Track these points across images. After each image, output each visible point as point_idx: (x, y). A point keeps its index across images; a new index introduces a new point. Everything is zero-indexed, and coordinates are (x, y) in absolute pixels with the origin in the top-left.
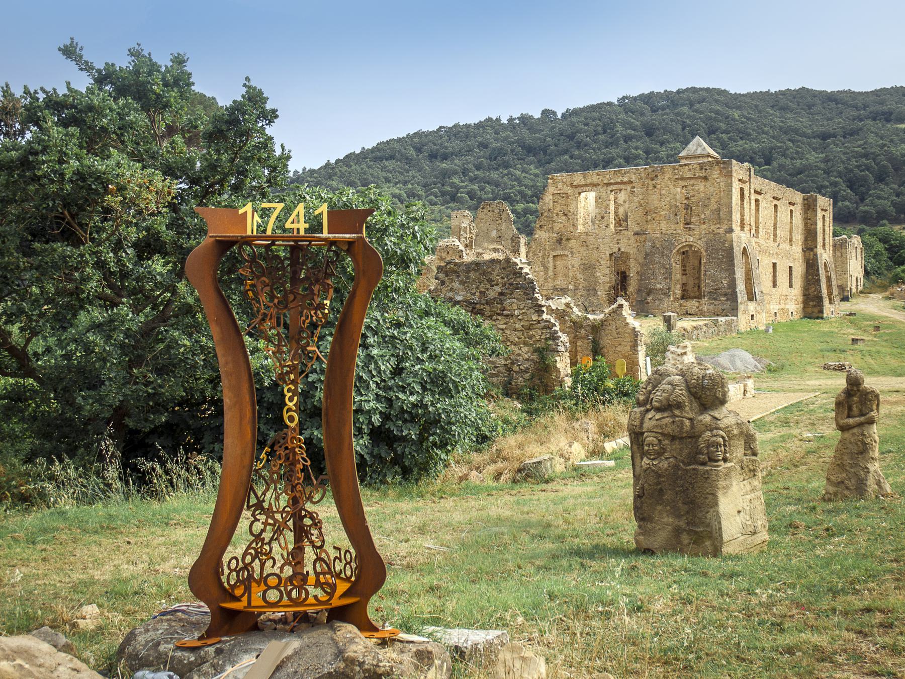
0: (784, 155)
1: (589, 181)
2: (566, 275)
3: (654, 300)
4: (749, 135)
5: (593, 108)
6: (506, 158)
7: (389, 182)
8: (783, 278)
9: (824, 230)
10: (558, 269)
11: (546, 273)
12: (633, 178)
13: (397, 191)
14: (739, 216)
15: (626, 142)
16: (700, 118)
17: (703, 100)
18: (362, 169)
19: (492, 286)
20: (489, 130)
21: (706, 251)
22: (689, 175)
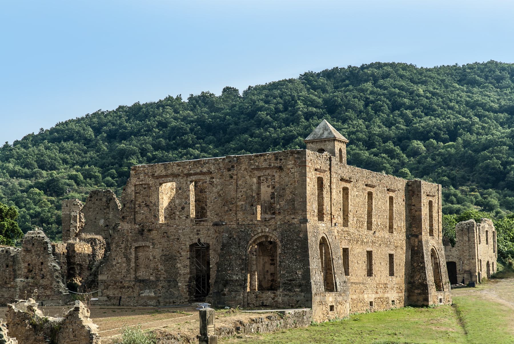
0: (470, 130)
1: (169, 172)
2: (147, 267)
3: (230, 291)
4: (435, 110)
5: (274, 86)
6: (185, 137)
7: (67, 163)
8: (381, 267)
9: (431, 217)
10: (140, 261)
11: (129, 265)
12: (213, 168)
13: (74, 173)
14: (315, 206)
15: (307, 119)
16: (384, 95)
18: (39, 150)
20: (169, 109)
21: (281, 241)
22: (264, 165)
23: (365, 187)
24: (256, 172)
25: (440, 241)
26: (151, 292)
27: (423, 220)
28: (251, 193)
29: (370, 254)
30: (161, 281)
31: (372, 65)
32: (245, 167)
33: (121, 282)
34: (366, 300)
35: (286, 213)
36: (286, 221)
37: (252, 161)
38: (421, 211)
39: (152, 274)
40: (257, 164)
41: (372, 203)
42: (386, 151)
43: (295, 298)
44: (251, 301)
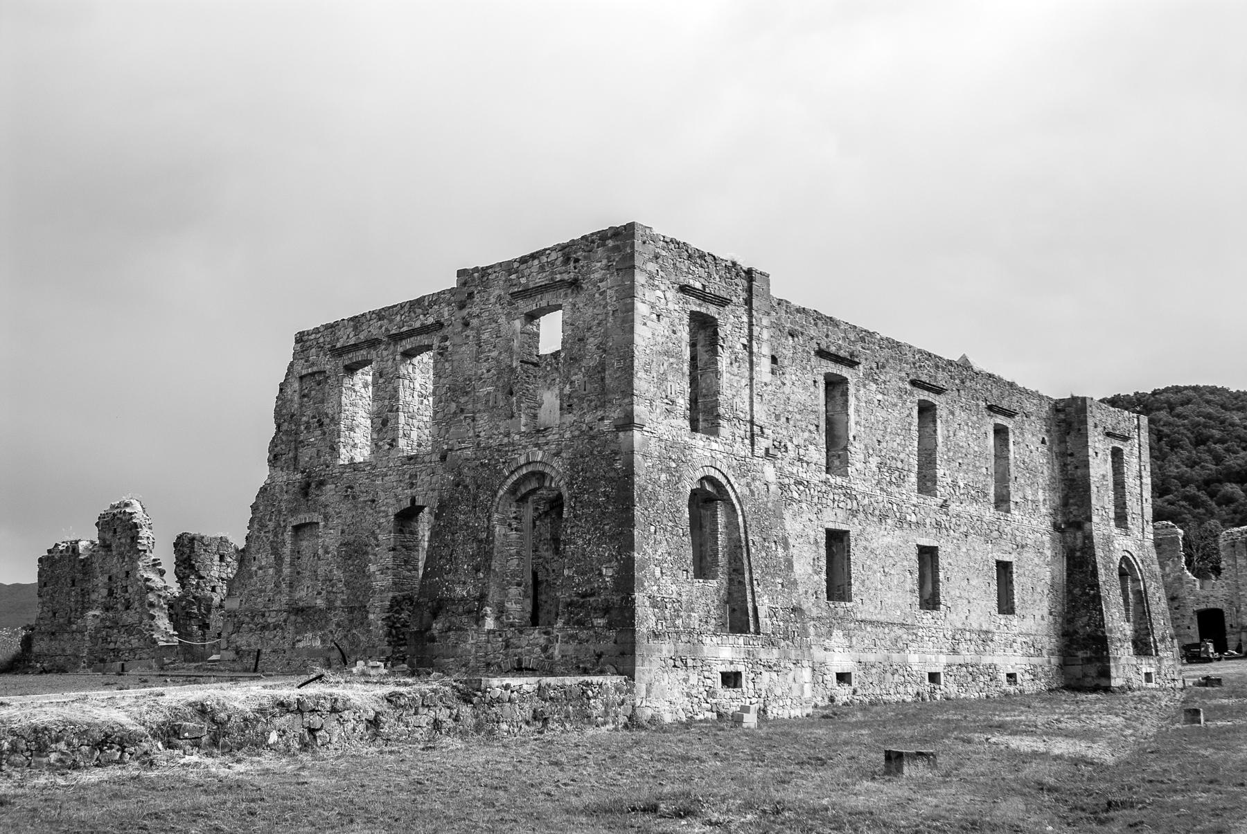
9: (1119, 485)
11: (279, 571)
16: (1183, 425)
17: (1189, 401)
22: (540, 279)
23: (908, 387)
24: (521, 303)
25: (1149, 543)
26: (314, 638)
27: (1093, 488)
28: (508, 361)
29: (928, 555)
30: (336, 608)
31: (1167, 390)
32: (497, 292)
33: (263, 615)
34: (915, 668)
35: (585, 405)
36: (584, 427)
37: (513, 277)
38: (1086, 465)
39: (319, 593)
40: (523, 281)
41: (935, 431)
42: (1186, 498)
43: (592, 647)
44: (495, 658)
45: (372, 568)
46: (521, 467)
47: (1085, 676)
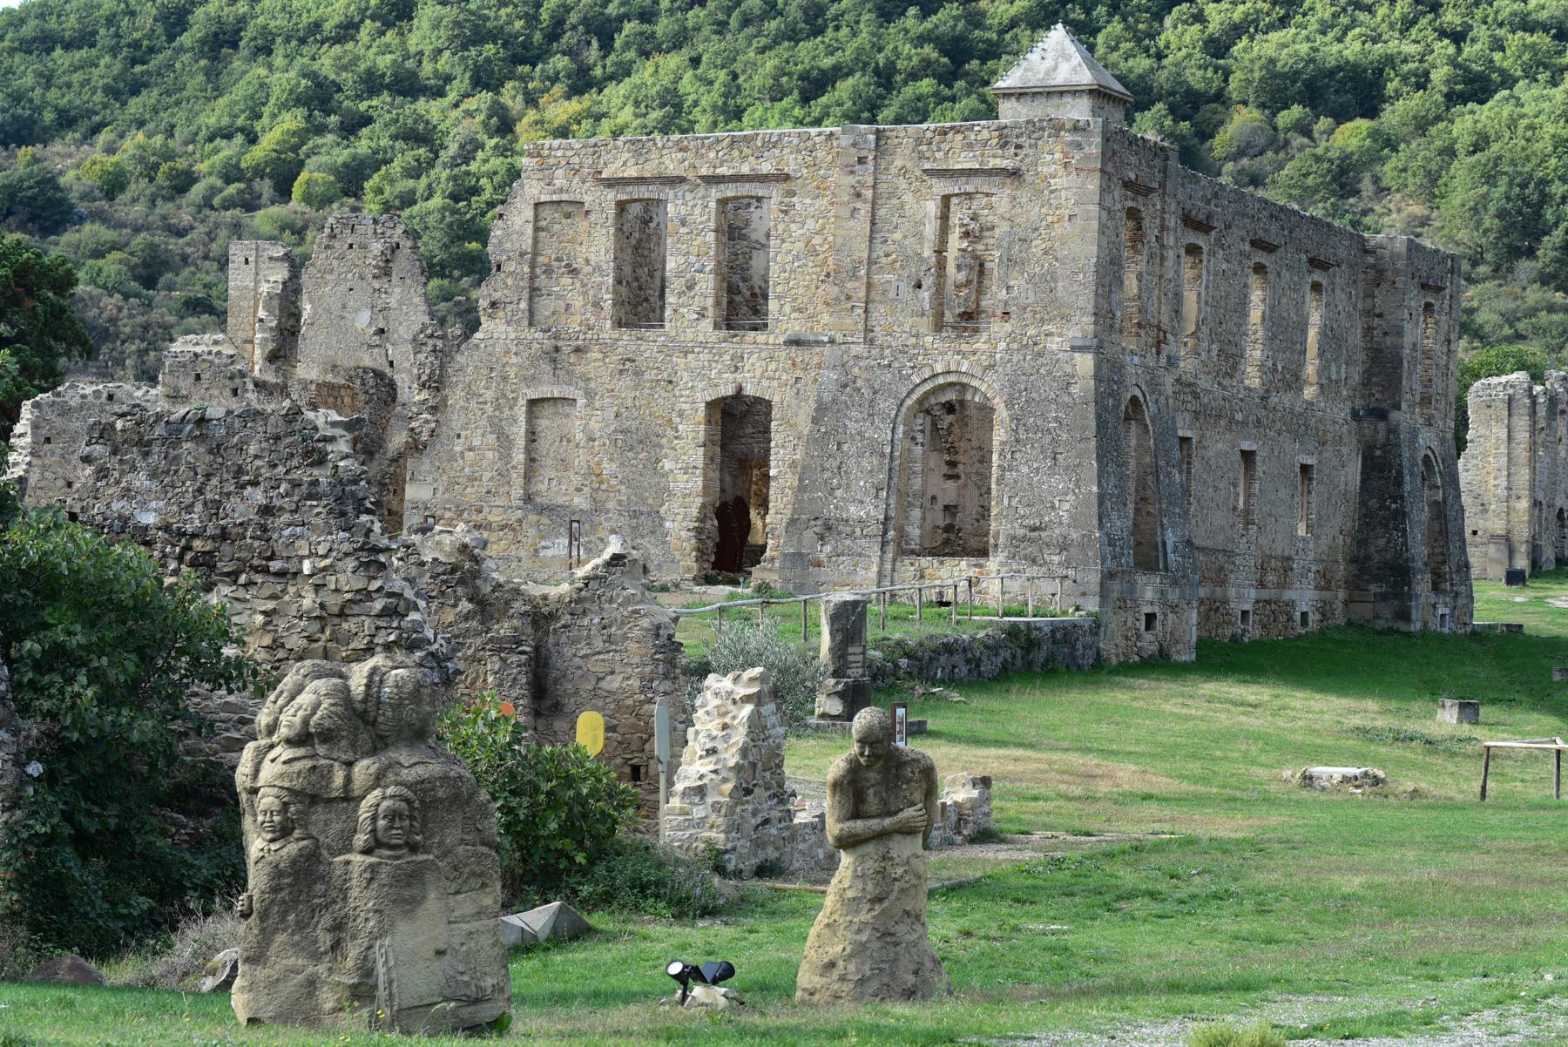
19: (243, 487)
21: (1009, 404)
35: (1028, 315)
37: (924, 148)
45: (668, 465)
46: (935, 376)
47: (1377, 616)
